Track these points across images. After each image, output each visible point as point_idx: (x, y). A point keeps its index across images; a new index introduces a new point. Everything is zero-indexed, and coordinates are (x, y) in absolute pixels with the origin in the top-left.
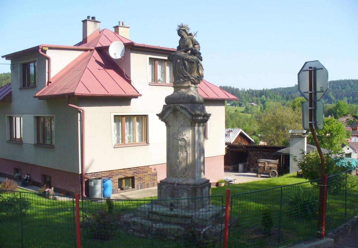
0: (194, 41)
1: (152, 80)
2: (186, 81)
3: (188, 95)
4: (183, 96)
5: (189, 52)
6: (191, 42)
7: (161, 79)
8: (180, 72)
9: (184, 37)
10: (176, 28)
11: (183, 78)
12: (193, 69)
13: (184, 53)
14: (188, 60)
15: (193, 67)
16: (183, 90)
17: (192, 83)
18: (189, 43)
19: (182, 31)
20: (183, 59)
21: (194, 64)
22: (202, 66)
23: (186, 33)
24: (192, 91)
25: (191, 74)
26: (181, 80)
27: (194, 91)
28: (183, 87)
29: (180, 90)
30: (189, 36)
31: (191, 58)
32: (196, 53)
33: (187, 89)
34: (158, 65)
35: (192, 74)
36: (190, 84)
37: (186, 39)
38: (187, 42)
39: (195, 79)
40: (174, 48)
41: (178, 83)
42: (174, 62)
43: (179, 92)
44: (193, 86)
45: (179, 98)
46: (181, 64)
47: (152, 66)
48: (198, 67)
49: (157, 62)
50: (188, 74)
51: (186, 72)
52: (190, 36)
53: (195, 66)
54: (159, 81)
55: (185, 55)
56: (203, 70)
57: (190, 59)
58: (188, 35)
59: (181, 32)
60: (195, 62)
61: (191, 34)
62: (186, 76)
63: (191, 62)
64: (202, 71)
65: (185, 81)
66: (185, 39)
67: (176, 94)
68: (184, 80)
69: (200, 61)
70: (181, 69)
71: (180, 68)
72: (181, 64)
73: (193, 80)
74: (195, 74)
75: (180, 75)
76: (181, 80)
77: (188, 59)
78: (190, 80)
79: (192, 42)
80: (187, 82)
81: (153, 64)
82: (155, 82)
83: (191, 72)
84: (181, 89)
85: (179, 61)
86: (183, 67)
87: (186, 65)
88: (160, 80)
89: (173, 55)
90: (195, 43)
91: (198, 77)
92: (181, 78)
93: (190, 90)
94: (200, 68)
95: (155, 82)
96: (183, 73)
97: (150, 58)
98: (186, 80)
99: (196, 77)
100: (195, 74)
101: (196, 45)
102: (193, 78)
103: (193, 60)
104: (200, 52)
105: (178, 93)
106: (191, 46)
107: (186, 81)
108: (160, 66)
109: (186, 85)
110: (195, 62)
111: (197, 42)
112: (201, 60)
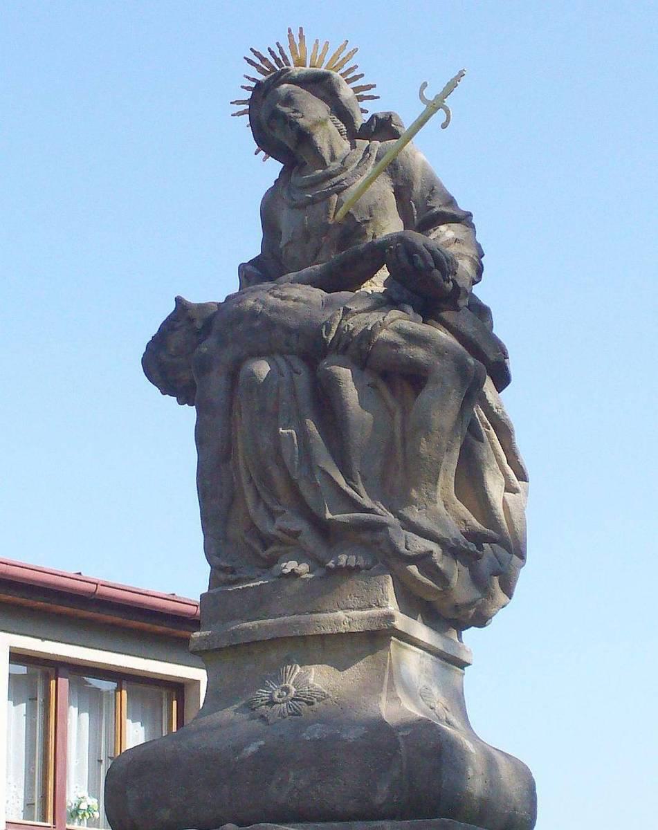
0: (417, 188)
1: (29, 805)
2: (350, 571)
3: (379, 726)
4: (315, 732)
5: (377, 283)
6: (384, 189)
7: (93, 802)
8: (280, 486)
9: (316, 151)
10: (237, 81)
11: (309, 539)
12: (424, 448)
13: (318, 295)
14: (360, 351)
15: (424, 427)
16: (317, 678)
17: (414, 602)
18: (366, 200)
19: (282, 109)
20: (311, 348)
21: (426, 396)
22: (504, 430)
23: (342, 113)
24: (408, 690)
25: (396, 499)
26: (290, 566)
27: (435, 691)
28: (304, 638)
29: (278, 679)
30: (363, 144)
31: (399, 331)
32: (432, 286)
33: (361, 664)
34: (73, 711)
35: (409, 501)
36: (392, 606)
37: (333, 166)
38: (348, 195)
39: (452, 551)
40: (182, 594)
41: (258, 604)
42: (216, 383)
43: (272, 703)
44: (421, 632)
45: (269, 762)
46: (294, 395)
47: (30, 714)
48: (473, 432)
49: (64, 682)
50: (367, 502)
51: (349, 477)
52: (377, 144)
53: (441, 410)
54: (75, 813)
55: (327, 305)
56: (522, 476)
57: (384, 334)
58: (353, 135)
59: (289, 100)
60: (442, 368)
61: (383, 127)
62: (342, 517)
63: (398, 377)
64: (510, 489)
65: (332, 577)
66: (322, 163)
67: (232, 723)
68: (317, 563)
69: (489, 386)
70: (292, 453)
71: (277, 436)
72: (294, 395)
73: (423, 560)
74: (442, 508)
75: (272, 515)
76: (290, 566)
77: (367, 335)
78: (388, 559)
79: (402, 192)
80: (352, 589)
81: (40, 700)
82: (44, 819)
83: (399, 473)
84: (289, 661)
85: (263, 368)
86: (312, 426)
87: (343, 406)
88: (84, 806)
89: (199, 324)
90: (427, 208)
91: (472, 536)
92: (290, 544)
93: (386, 678)
94: (486, 453)
95: (44, 819)
96: (308, 494)
97: (17, 657)
98: (343, 559)
99: (454, 531)
100: (440, 506)
101: (443, 228)
102: (421, 545)
103: (420, 354)
104: (485, 300)
105: (250, 707)
106: (391, 225)
107: (350, 571)
108: (85, 716)
109: (346, 617)
110: (442, 368)
111: (451, 202)
112: (502, 379)
